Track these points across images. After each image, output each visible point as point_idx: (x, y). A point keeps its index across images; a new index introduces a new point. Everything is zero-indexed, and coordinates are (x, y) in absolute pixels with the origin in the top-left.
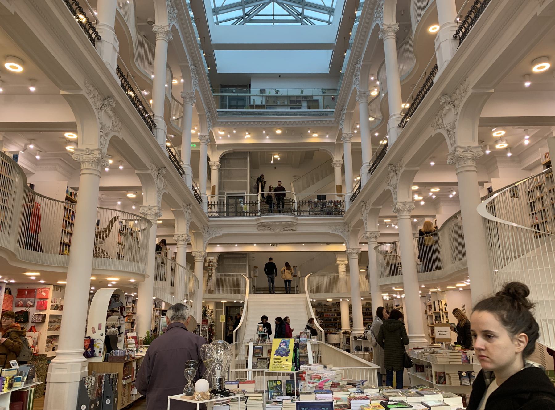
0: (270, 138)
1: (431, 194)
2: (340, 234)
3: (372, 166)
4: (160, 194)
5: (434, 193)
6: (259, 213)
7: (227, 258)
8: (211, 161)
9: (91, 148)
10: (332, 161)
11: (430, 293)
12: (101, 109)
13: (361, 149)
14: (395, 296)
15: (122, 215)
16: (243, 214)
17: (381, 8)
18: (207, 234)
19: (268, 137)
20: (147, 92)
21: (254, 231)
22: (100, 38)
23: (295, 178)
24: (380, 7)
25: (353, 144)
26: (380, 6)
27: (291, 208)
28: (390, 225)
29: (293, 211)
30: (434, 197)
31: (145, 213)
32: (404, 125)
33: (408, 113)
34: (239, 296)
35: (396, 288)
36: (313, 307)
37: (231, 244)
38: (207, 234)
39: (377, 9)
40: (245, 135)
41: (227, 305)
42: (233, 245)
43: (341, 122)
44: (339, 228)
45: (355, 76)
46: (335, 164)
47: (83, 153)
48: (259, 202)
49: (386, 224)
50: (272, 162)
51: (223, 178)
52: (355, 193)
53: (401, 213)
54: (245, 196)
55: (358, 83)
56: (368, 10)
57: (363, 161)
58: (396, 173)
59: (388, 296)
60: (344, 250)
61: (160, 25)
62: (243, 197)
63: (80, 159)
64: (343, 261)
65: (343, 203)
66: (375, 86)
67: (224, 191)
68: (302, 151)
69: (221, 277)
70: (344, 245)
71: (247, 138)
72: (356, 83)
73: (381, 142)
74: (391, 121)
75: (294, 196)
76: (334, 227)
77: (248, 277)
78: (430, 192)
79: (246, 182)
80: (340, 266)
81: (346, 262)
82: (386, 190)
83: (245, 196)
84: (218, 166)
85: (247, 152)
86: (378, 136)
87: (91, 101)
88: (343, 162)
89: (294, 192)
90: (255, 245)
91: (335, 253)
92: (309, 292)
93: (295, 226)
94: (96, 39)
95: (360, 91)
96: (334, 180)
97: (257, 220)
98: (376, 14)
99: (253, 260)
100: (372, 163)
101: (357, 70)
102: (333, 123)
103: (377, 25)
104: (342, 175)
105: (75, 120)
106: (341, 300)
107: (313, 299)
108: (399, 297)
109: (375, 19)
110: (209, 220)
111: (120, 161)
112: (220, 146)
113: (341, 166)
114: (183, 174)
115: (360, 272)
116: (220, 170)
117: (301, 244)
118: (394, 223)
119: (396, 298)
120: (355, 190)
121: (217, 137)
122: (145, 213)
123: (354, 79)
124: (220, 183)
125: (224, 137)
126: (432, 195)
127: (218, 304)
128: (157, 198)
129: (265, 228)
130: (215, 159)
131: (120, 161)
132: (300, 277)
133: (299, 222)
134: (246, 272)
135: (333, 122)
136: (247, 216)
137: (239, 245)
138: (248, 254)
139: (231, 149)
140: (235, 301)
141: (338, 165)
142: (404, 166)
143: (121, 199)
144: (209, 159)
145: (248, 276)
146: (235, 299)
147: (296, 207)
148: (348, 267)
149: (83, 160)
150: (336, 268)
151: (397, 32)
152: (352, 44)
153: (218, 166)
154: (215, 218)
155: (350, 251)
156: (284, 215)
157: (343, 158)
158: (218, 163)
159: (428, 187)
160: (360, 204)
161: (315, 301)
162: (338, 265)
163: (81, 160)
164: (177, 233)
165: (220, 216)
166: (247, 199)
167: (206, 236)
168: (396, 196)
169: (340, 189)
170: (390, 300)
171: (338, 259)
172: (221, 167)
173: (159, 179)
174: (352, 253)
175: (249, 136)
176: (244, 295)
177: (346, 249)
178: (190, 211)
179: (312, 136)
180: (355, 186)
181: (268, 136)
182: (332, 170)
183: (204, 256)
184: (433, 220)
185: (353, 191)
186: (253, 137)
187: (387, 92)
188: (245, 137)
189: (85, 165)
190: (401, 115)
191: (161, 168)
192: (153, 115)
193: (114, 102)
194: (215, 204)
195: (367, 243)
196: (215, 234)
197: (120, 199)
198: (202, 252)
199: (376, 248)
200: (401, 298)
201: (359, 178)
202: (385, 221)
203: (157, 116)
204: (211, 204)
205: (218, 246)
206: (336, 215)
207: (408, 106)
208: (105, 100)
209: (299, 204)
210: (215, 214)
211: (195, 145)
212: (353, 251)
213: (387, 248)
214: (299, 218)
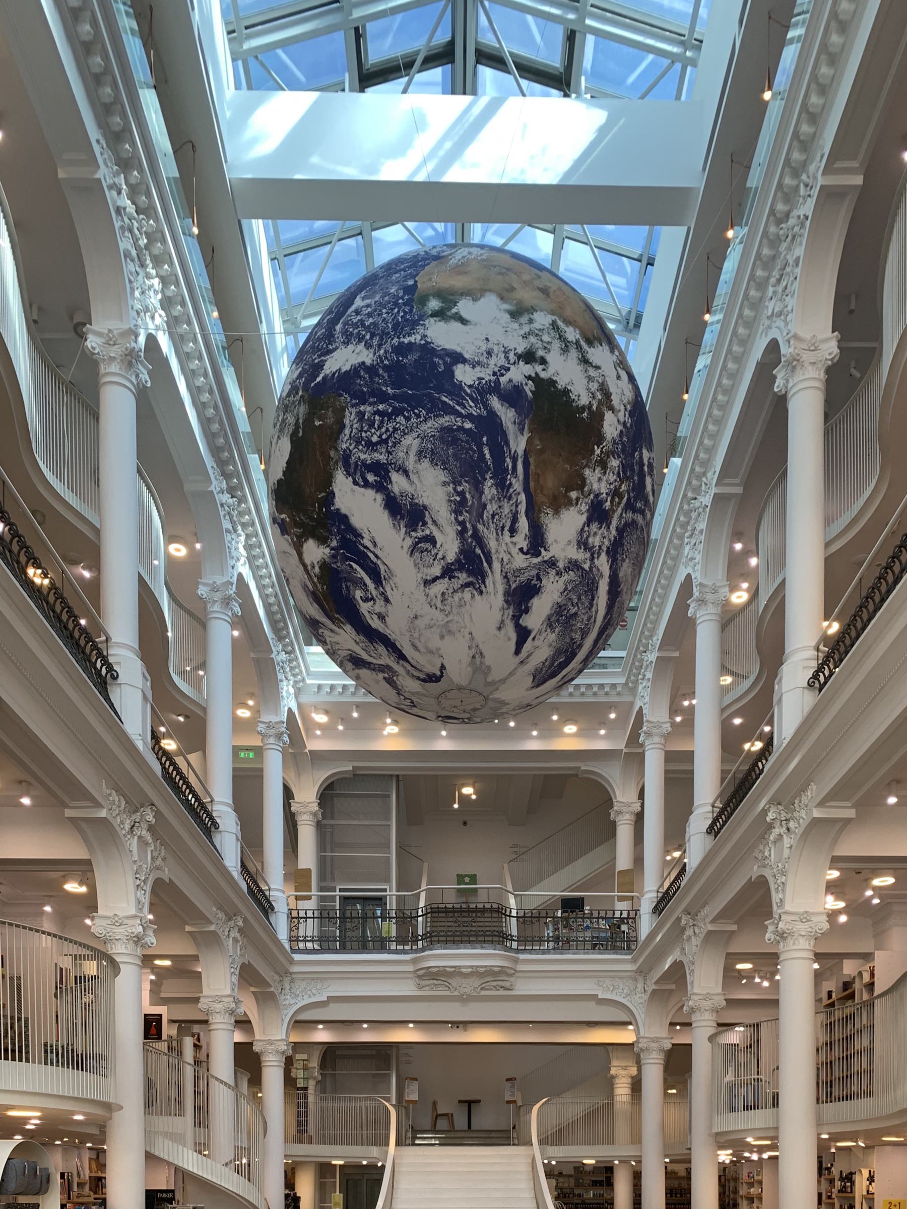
2: (624, 1001)
3: (719, 812)
4: (145, 882)
5: (878, 890)
6: (420, 943)
8: (296, 800)
10: (612, 806)
11: (833, 1150)
13: (692, 772)
14: (747, 1154)
16: (381, 944)
17: (792, 278)
18: (288, 997)
21: (408, 988)
23: (516, 853)
24: (788, 274)
25: (670, 757)
26: (788, 269)
27: (502, 932)
30: (876, 901)
32: (825, 683)
34: (375, 1151)
36: (548, 1175)
38: (288, 997)
39: (779, 281)
40: (385, 724)
43: (640, 687)
44: (621, 986)
45: (691, 536)
48: (420, 913)
50: (456, 806)
51: (328, 847)
52: (667, 892)
55: (698, 557)
56: (747, 289)
57: (786, 647)
58: (788, 829)
60: (631, 1042)
62: (380, 901)
66: (742, 575)
67: (332, 884)
68: (534, 775)
69: (329, 1104)
70: (631, 1027)
71: (390, 735)
72: (692, 559)
73: (747, 746)
74: (786, 669)
76: (608, 982)
79: (388, 860)
80: (617, 1081)
81: (634, 1071)
83: (386, 896)
84: (315, 814)
85: (392, 776)
86: (741, 725)
88: (639, 809)
89: (510, 888)
91: (610, 1048)
92: (541, 1142)
93: (511, 979)
95: (701, 585)
97: (414, 961)
98: (773, 301)
99: (408, 1062)
100: (719, 804)
101: (699, 514)
102: (619, 694)
103: (773, 346)
106: (616, 1162)
108: (755, 1157)
109: (767, 322)
110: (293, 959)
111: (20, 782)
112: (318, 757)
113: (633, 818)
115: (666, 1094)
116: (319, 826)
117: (525, 1025)
118: (762, 974)
119: (748, 1160)
120: (667, 884)
123: (687, 548)
124: (322, 862)
126: (872, 897)
127: (324, 1170)
128: (136, 894)
129: (435, 981)
131: (20, 782)
132: (520, 1106)
133: (520, 967)
135: (619, 689)
137: (418, 1025)
138: (394, 1050)
140: (365, 1163)
143: (52, 899)
145: (394, 1102)
146: (364, 1155)
147: (513, 927)
148: (636, 1086)
150: (610, 1083)
151: (834, 365)
152: (685, 438)
153: (315, 814)
154: (308, 953)
156: (482, 948)
158: (315, 807)
161: (554, 1163)
162: (613, 1077)
164: (206, 991)
165: (321, 951)
166: (392, 904)
167: (287, 1003)
168: (781, 896)
171: (614, 1063)
172: (324, 815)
175: (395, 729)
176: (384, 1148)
177: (634, 1039)
178: (237, 935)
180: (669, 874)
182: (611, 831)
183: (283, 1052)
184: (864, 965)
185: (662, 885)
186: (404, 733)
187: (785, 579)
188: (385, 733)
192: (107, 641)
194: (306, 918)
196: (310, 996)
197: (48, 899)
198: (280, 1043)
199: (711, 1039)
200: (760, 1159)
201: (677, 854)
202: (740, 966)
203: (118, 645)
204: (294, 919)
206: (615, 949)
207: (835, 628)
209: (527, 919)
210: (309, 945)
211: (251, 755)
212: (653, 1045)
214: (522, 956)
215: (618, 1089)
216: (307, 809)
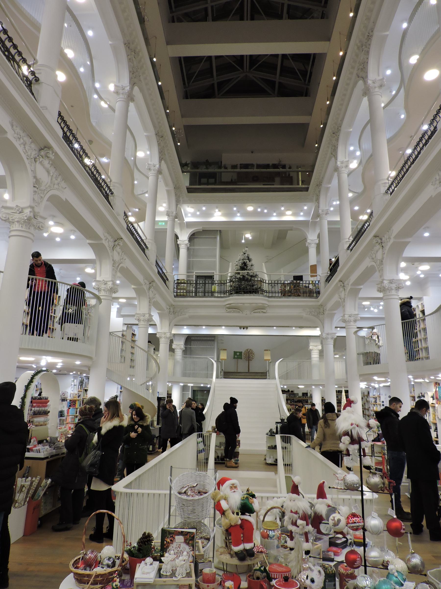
0: (242, 216)
1: (419, 272)
5: (423, 272)
7: (194, 340)
9: (22, 206)
10: (306, 241)
12: (35, 160)
14: (373, 384)
15: (63, 287)
16: (212, 294)
19: (239, 214)
20: (107, 159)
22: (37, 79)
28: (369, 308)
29: (263, 292)
30: (422, 276)
31: (98, 288)
33: (398, 180)
35: (379, 377)
37: (198, 326)
40: (215, 212)
41: (195, 389)
42: (199, 327)
46: (310, 244)
47: (13, 211)
48: (228, 282)
49: (364, 307)
50: (243, 241)
53: (388, 292)
54: (214, 275)
59: (366, 385)
61: (121, 86)
63: (9, 218)
64: (316, 346)
65: (318, 284)
75: (266, 276)
77: (215, 361)
78: (417, 270)
79: (215, 262)
80: (313, 352)
81: (320, 347)
82: (369, 266)
84: (186, 245)
85: (217, 230)
87: (20, 149)
88: (318, 242)
89: (265, 271)
90: (223, 327)
92: (279, 378)
94: (33, 81)
96: (308, 261)
99: (222, 343)
100: (352, 239)
104: (317, 255)
105: (4, 174)
107: (284, 385)
111: (72, 230)
112: (190, 224)
114: (146, 249)
116: (188, 249)
121: (186, 215)
122: (98, 288)
125: (194, 215)
130: (184, 238)
131: (72, 230)
132: (270, 362)
134: (214, 356)
136: (215, 297)
139: (200, 228)
140: (202, 385)
141: (313, 245)
142: (392, 237)
144: (177, 237)
148: (321, 353)
149: (12, 220)
150: (308, 354)
153: (186, 245)
155: (324, 336)
157: (319, 237)
158: (187, 242)
159: (416, 264)
160: (337, 284)
163: (10, 220)
169: (314, 269)
170: (366, 388)
172: (190, 245)
173: (115, 251)
174: (327, 338)
175: (220, 213)
177: (320, 334)
179: (285, 213)
181: (239, 213)
186: (224, 215)
189: (14, 226)
190: (388, 180)
191: (118, 239)
193: (52, 153)
195: (344, 328)
199: (356, 332)
205: (185, 327)
208: (41, 150)
213: (363, 333)
215: (313, 355)
216: (184, 243)
